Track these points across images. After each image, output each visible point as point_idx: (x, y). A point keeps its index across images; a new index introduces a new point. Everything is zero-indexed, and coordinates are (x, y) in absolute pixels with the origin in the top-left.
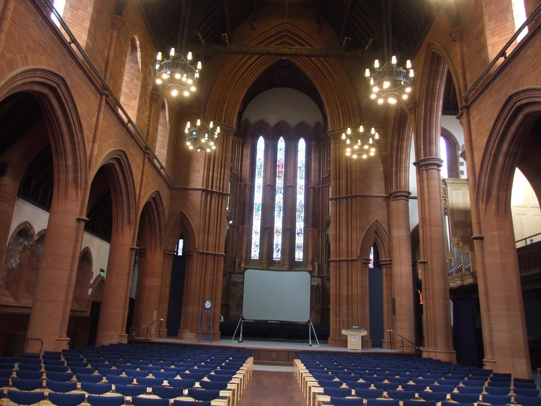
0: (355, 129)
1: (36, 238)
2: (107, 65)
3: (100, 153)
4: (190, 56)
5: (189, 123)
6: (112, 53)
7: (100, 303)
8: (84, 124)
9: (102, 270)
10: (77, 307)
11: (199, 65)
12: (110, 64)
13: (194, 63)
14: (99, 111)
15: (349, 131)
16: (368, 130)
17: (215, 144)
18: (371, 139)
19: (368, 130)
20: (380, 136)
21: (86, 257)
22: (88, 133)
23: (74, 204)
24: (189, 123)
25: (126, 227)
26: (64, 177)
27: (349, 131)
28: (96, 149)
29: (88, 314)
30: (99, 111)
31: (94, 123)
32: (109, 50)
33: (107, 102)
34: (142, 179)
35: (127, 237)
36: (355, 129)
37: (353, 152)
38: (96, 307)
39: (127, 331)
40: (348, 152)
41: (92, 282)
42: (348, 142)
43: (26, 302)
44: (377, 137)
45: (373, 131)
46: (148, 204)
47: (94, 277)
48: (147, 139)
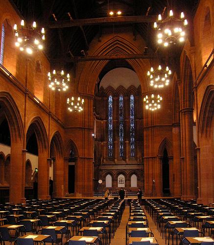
0: (155, 68)
1: (6, 158)
2: (26, 80)
3: (28, 120)
4: (34, 25)
5: (68, 99)
6: (28, 73)
7: (37, 183)
8: (20, 110)
9: (36, 169)
10: (27, 186)
11: (43, 31)
12: (28, 78)
13: (39, 29)
14: (25, 102)
15: (152, 70)
16: (164, 68)
17: (82, 108)
18: (166, 75)
19: (164, 68)
20: (174, 14)
21: (28, 163)
22: (22, 113)
23: (20, 145)
24: (68, 99)
25: (18, 139)
26: (13, 134)
27: (152, 70)
28: (26, 119)
29: (33, 188)
30: (25, 102)
31: (24, 108)
32: (27, 72)
33: (28, 97)
34: (49, 127)
35: (45, 155)
36: (155, 68)
37: (155, 83)
38: (36, 184)
39: (51, 194)
40: (152, 83)
41: (32, 174)
42: (151, 77)
43: (6, 185)
44: (170, 73)
45: (167, 69)
46: (32, 125)
47: (33, 172)
48: (50, 108)
